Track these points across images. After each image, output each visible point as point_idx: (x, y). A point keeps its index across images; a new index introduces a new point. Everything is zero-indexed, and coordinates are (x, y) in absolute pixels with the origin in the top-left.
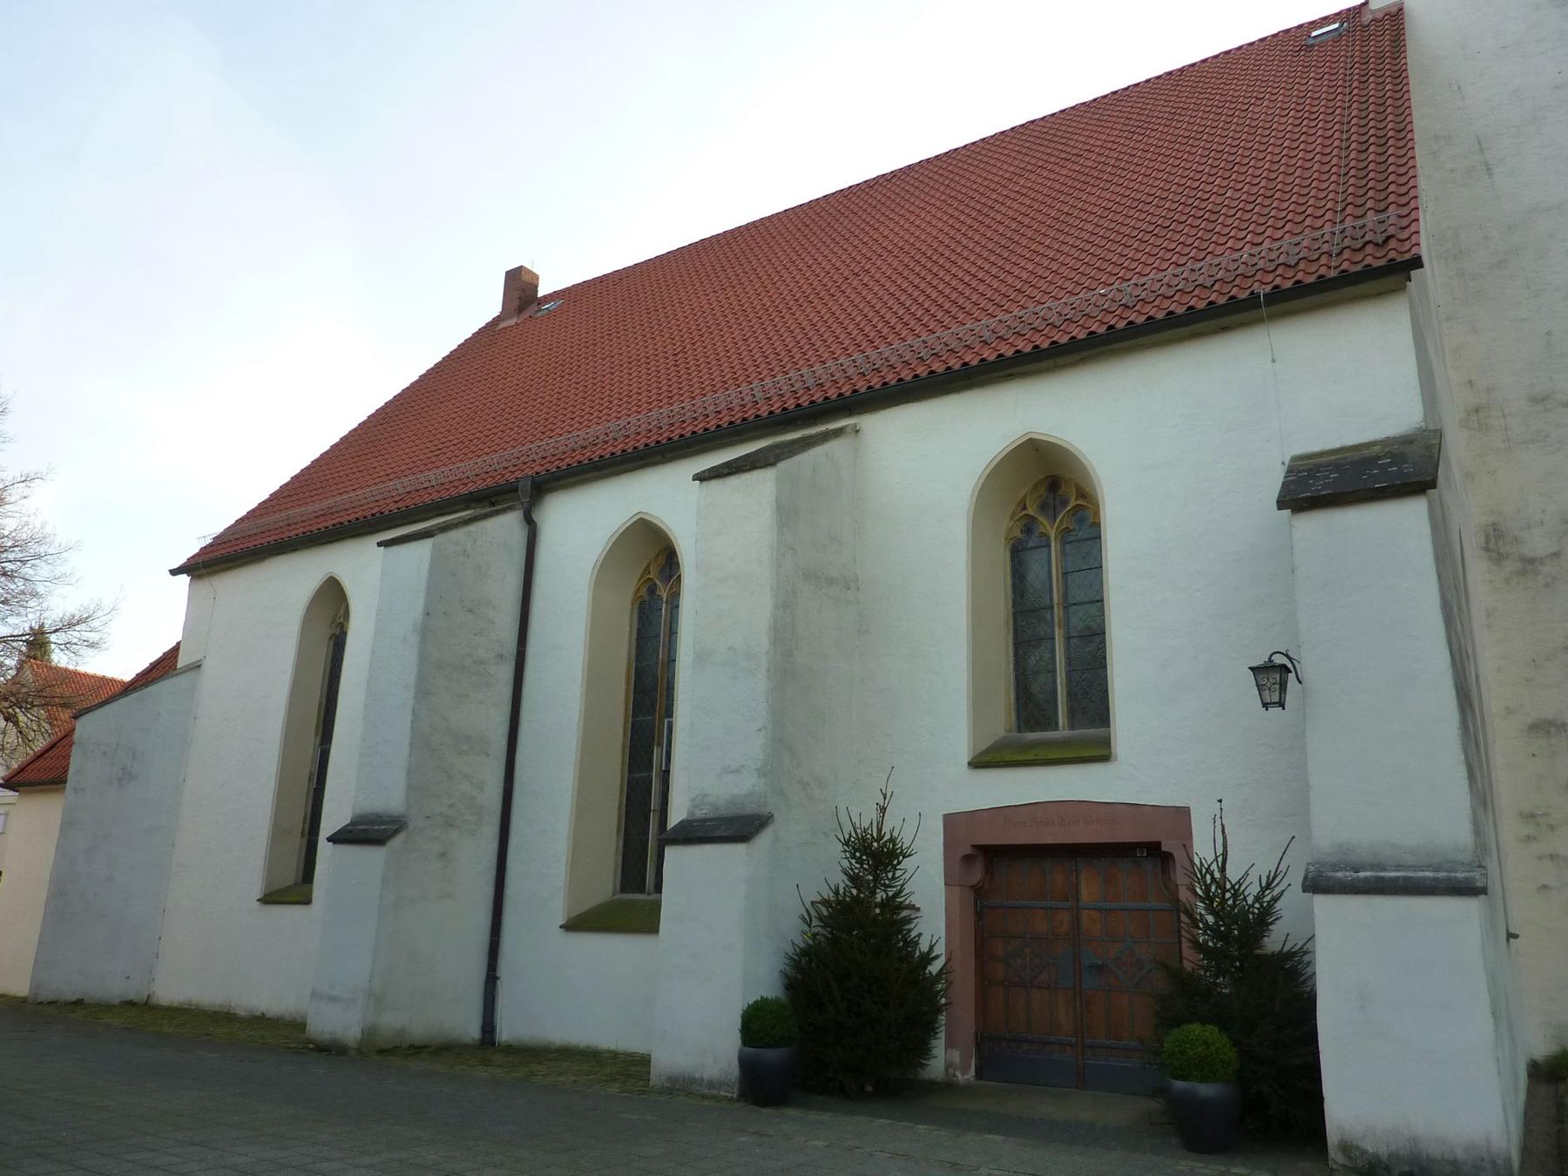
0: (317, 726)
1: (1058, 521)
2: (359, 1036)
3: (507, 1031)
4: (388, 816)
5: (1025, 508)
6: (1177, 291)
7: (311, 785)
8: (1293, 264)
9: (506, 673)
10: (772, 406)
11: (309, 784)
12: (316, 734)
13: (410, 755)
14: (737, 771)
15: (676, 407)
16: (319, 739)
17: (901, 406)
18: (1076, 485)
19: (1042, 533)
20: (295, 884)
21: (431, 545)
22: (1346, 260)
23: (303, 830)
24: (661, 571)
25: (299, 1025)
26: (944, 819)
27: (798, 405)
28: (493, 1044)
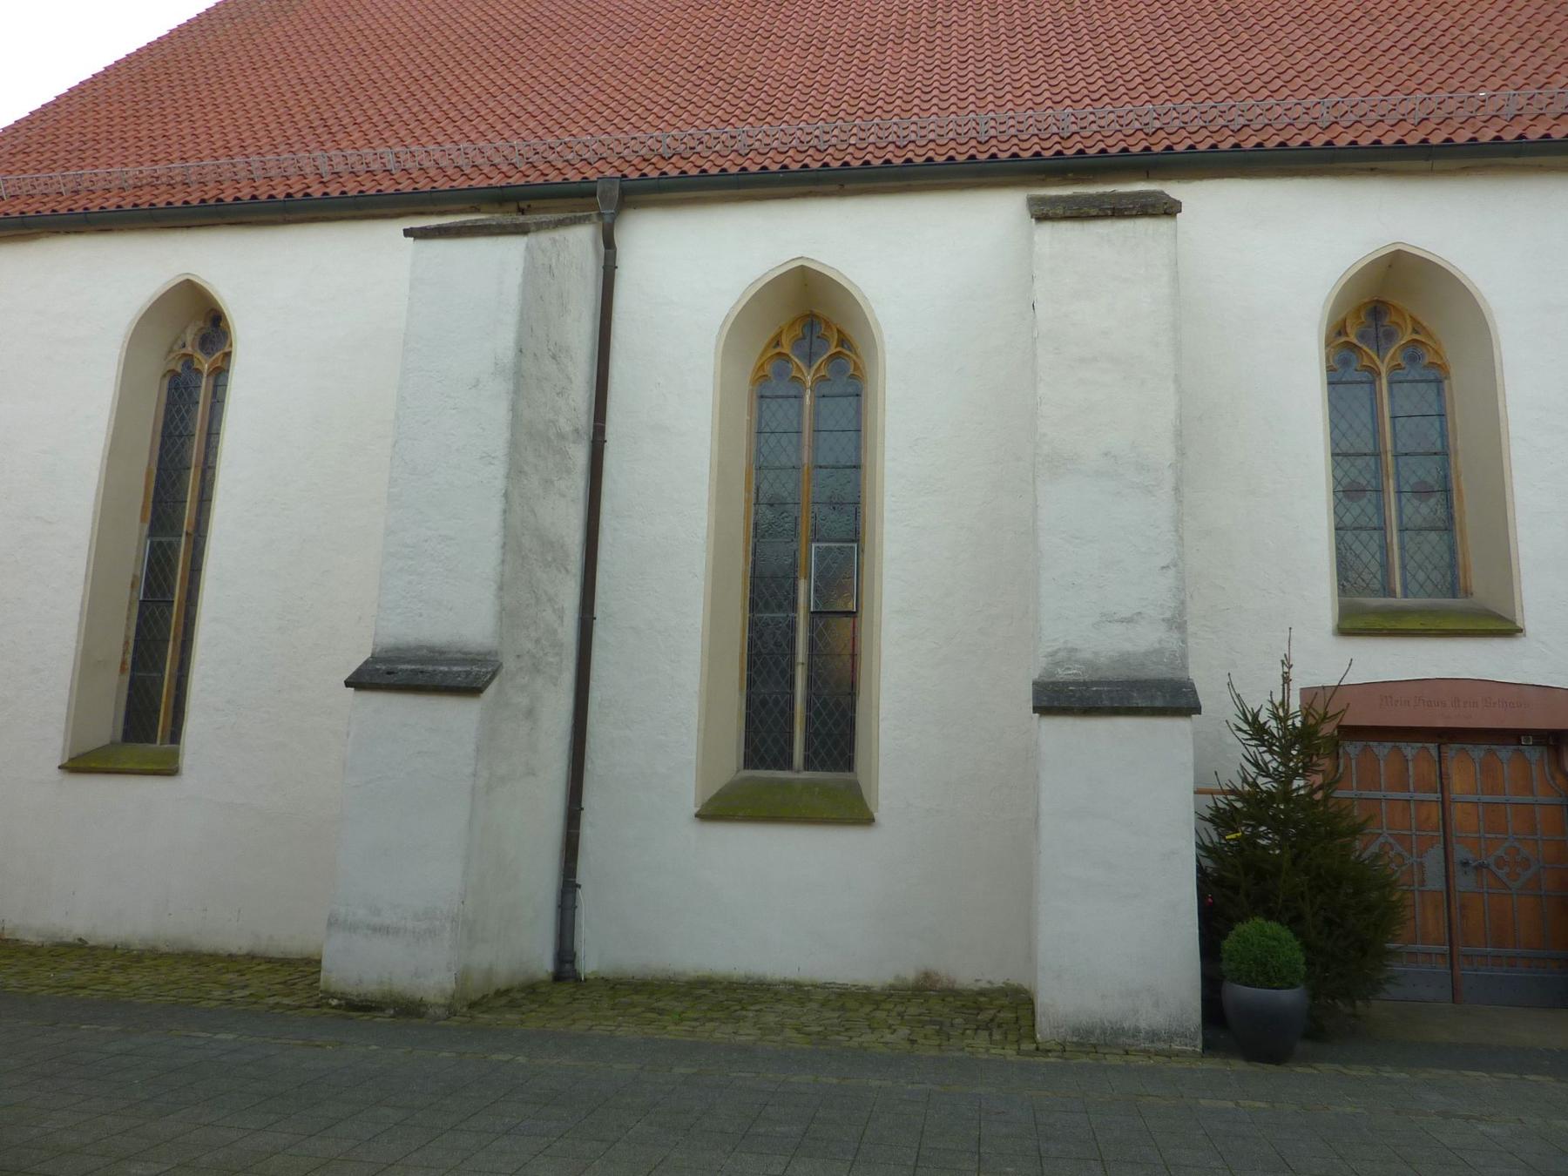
0: (144, 507)
1: (815, 367)
2: (450, 985)
3: (590, 962)
4: (460, 652)
5: (778, 344)
6: (732, 151)
7: (135, 594)
8: (983, 141)
9: (580, 455)
10: (189, 194)
11: (131, 594)
12: (143, 520)
13: (503, 562)
14: (1129, 620)
15: (101, 171)
16: (146, 526)
17: (1225, 180)
18: (839, 331)
19: (793, 377)
20: (112, 743)
21: (524, 245)
22: (952, 149)
23: (123, 663)
24: (797, 343)
25: (310, 965)
26: (1301, 693)
27: (254, 197)
28: (576, 978)
